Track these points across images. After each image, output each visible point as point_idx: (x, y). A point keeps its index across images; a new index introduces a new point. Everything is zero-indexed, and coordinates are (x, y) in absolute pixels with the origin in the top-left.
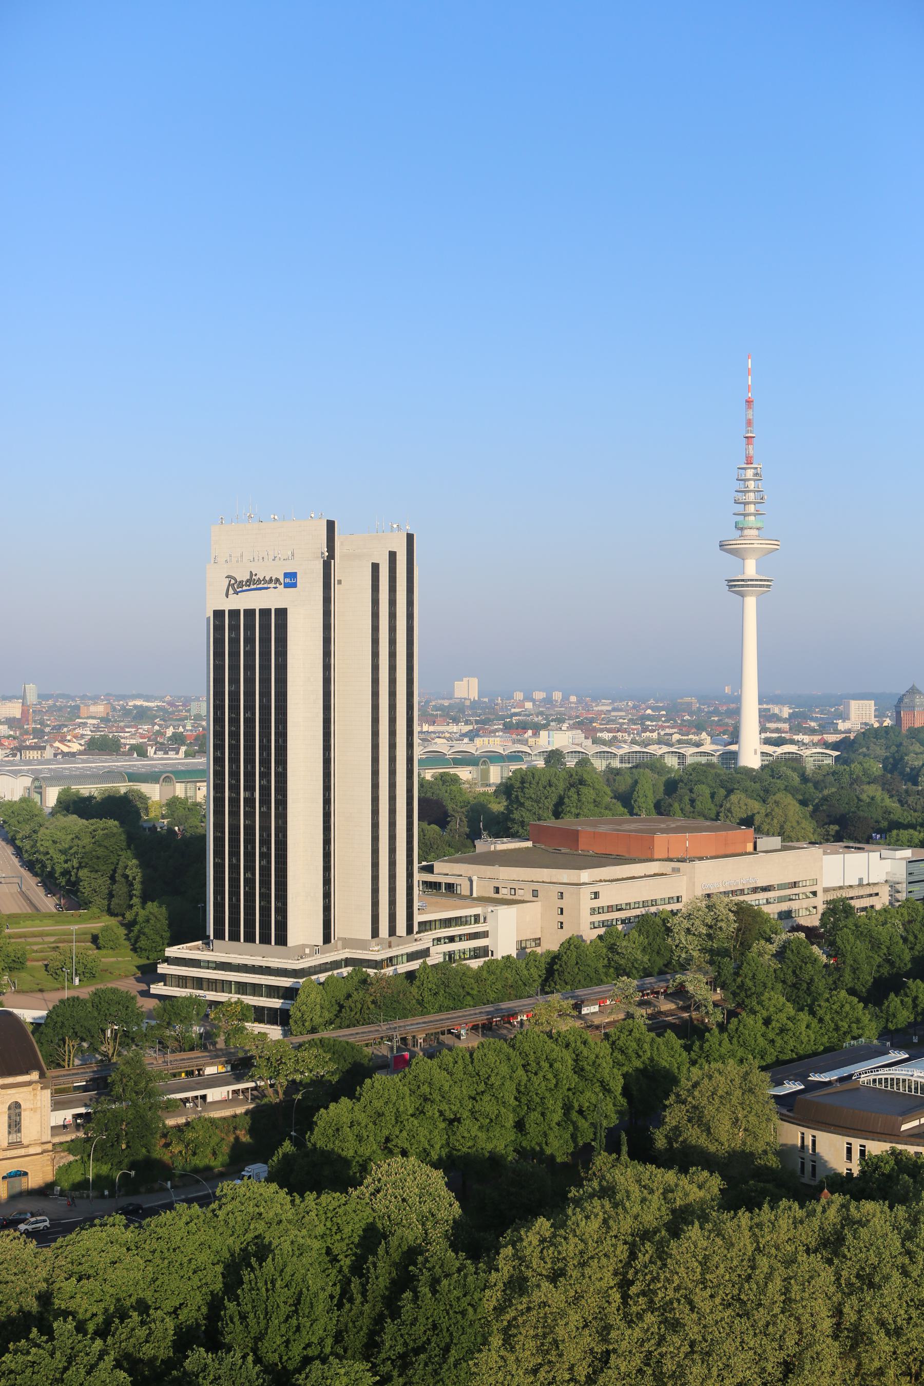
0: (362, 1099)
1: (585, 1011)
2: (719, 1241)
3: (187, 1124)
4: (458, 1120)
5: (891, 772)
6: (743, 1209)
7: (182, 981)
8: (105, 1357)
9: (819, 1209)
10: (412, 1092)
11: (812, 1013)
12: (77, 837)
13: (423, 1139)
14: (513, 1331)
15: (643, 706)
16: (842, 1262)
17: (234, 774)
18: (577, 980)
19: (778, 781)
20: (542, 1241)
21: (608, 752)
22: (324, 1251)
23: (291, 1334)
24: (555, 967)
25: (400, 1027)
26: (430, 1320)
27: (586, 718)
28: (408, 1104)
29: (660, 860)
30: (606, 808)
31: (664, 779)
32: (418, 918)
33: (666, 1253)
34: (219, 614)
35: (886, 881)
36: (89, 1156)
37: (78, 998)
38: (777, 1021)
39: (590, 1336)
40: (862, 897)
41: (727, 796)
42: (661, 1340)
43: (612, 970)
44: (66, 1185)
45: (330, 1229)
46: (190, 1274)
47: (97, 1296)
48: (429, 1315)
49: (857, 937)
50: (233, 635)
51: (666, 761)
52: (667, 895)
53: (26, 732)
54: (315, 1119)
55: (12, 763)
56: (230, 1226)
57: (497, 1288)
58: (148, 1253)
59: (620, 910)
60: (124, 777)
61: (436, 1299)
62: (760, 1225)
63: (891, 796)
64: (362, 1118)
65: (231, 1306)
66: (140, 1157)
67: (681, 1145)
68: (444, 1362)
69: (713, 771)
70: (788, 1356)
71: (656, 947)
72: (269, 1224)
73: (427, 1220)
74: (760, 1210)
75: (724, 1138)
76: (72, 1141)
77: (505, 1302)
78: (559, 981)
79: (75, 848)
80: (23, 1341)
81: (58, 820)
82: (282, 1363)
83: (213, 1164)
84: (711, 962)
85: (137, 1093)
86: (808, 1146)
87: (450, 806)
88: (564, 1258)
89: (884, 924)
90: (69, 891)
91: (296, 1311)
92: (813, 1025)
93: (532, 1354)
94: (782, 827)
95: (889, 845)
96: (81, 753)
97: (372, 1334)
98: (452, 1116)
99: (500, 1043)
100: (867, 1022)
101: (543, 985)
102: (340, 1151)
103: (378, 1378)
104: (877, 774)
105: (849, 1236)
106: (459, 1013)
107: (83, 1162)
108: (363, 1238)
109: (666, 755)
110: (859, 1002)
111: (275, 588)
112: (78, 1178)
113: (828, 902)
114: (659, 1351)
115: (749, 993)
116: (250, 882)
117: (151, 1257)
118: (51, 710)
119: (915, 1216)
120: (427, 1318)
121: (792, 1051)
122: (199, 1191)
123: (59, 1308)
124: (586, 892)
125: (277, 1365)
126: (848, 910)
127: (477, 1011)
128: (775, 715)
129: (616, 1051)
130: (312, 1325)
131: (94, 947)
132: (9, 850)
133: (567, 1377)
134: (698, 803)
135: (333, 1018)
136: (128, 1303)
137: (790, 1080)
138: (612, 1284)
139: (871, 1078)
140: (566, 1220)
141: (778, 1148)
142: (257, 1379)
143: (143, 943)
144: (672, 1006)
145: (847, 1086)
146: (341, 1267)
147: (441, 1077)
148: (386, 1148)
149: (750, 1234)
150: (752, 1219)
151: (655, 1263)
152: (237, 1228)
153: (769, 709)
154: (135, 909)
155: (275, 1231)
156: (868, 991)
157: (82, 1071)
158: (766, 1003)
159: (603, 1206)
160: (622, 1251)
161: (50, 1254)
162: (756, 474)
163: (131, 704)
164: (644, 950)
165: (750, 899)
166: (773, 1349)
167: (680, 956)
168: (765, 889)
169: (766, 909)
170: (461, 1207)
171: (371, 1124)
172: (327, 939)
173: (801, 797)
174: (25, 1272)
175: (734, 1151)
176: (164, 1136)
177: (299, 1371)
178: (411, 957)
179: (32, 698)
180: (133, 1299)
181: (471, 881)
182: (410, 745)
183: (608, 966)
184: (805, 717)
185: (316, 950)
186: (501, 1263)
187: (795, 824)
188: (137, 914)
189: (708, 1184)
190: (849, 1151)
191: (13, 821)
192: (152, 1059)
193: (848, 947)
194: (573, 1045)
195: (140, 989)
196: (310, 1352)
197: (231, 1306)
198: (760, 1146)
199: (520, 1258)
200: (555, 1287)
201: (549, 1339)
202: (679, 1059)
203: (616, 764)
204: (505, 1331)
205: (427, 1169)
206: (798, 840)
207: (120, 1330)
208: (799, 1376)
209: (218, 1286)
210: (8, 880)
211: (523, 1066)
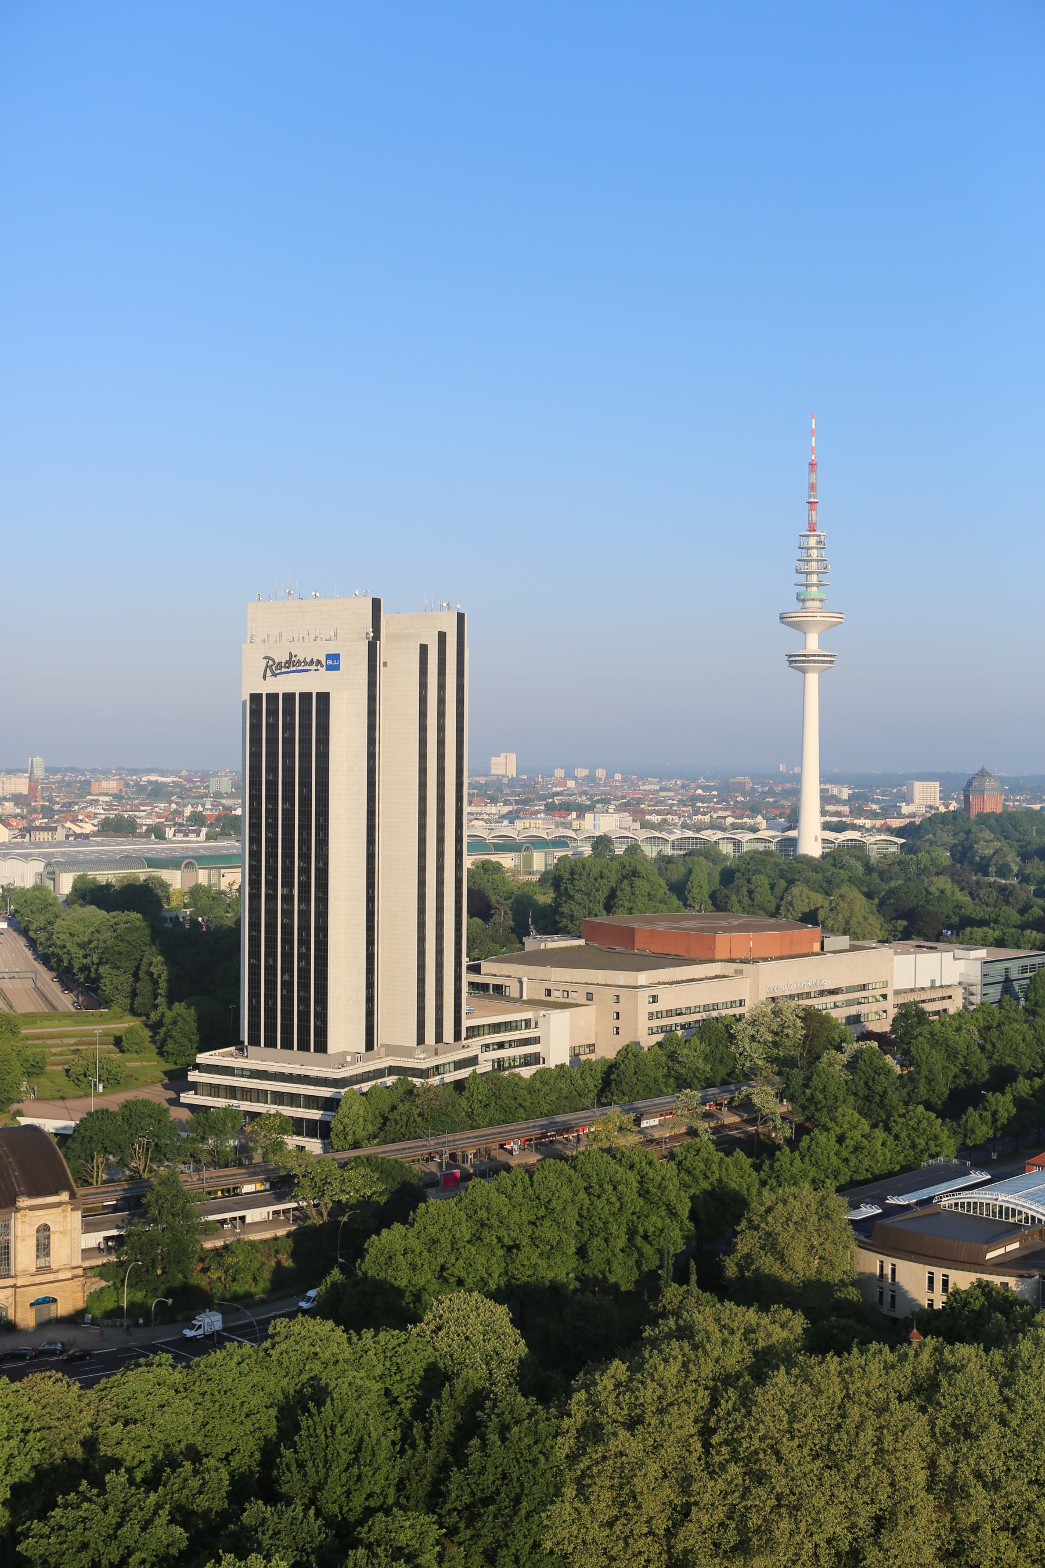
0: (416, 1225)
1: (644, 1124)
2: (807, 1388)
3: (226, 1247)
4: (517, 1247)
5: (960, 861)
6: (831, 1353)
7: (215, 1090)
8: (160, 1512)
9: (912, 1353)
10: (469, 1217)
11: (888, 1129)
12: (97, 931)
13: (480, 1268)
14: (588, 1481)
15: (693, 785)
16: (936, 1411)
17: (271, 870)
19: (841, 871)
20: (618, 1385)
22: (382, 1392)
23: (351, 1483)
24: (612, 1077)
25: (449, 1141)
26: (500, 1470)
27: (632, 799)
28: (464, 1229)
29: (721, 961)
30: (661, 902)
31: (719, 868)
32: (466, 1023)
33: (751, 1400)
34: (255, 698)
35: (960, 983)
36: (123, 1281)
37: (107, 1111)
38: (852, 1138)
39: (670, 1487)
40: (934, 1000)
41: (787, 889)
42: (746, 1492)
43: (672, 1080)
44: (98, 1313)
46: (243, 1418)
47: (144, 1443)
49: (933, 1046)
50: (271, 721)
52: (729, 999)
53: (34, 811)
54: (366, 1246)
55: (21, 846)
56: (284, 1366)
57: (570, 1435)
58: (198, 1396)
59: (679, 1014)
60: (142, 862)
62: (849, 1371)
63: (962, 889)
64: (416, 1244)
65: (288, 1454)
66: (177, 1284)
68: (515, 1514)
69: (772, 860)
70: (881, 1510)
71: (719, 1056)
72: (325, 1364)
73: (492, 1359)
75: (799, 1266)
76: (104, 1265)
77: (578, 1449)
78: (616, 1092)
80: (73, 1494)
81: (75, 912)
82: (342, 1515)
83: (253, 1290)
84: (779, 1073)
85: (173, 1215)
87: (493, 899)
88: (642, 1405)
89: (958, 1029)
90: (89, 988)
91: (356, 1459)
92: (889, 1143)
93: (608, 1506)
94: (847, 923)
95: (961, 943)
96: (95, 834)
97: (436, 1483)
98: (511, 1243)
99: (562, 1165)
100: (945, 1139)
101: (600, 1094)
103: (444, 1531)
104: (945, 864)
105: (945, 1383)
107: (116, 1289)
108: (424, 1379)
109: (721, 842)
110: (937, 1118)
112: (111, 1305)
113: (901, 1006)
114: (743, 1504)
115: (819, 1106)
116: (287, 985)
118: (63, 784)
119: (1012, 1360)
120: (496, 1467)
121: (867, 1170)
122: (239, 1320)
123: (105, 1455)
124: (644, 996)
125: (336, 1516)
126: (921, 1015)
127: (531, 1125)
128: (834, 797)
129: (683, 1172)
130: (374, 1474)
132: (22, 942)
133: (645, 1530)
134: (757, 897)
135: (377, 1131)
136: (177, 1449)
137: (867, 1203)
138: (693, 1431)
139: (953, 1202)
140: (643, 1364)
141: (856, 1277)
142: (319, 1534)
143: (170, 1046)
144: (737, 1119)
145: (928, 1210)
146: (401, 1409)
147: (499, 1201)
148: (440, 1276)
149: (839, 1379)
150: (841, 1364)
151: (739, 1410)
152: (292, 1369)
153: (827, 790)
154: (160, 1009)
155: (333, 1372)
156: (944, 1103)
157: (112, 1189)
158: (840, 1119)
159: (681, 1348)
160: (703, 1398)
161: (94, 1397)
162: (820, 542)
163: (144, 779)
164: (706, 1058)
165: (817, 1003)
166: (864, 1503)
167: (744, 1065)
168: (833, 992)
169: (835, 1014)
170: (527, 1345)
171: (425, 1252)
172: (370, 1045)
173: (866, 890)
174: (68, 1417)
175: (809, 1281)
176: (202, 1260)
177: (361, 1523)
178: (459, 1065)
179: (39, 773)
180: (183, 1445)
181: (521, 983)
183: (668, 1076)
184: (865, 798)
185: (357, 1058)
186: (573, 1408)
187: (861, 919)
188: (163, 1015)
189: (791, 1323)
190: (931, 1280)
191: (26, 911)
192: (189, 1178)
193: (924, 1057)
194: (638, 1166)
195: (168, 1097)
196: (372, 1503)
197: (288, 1454)
198: (836, 1276)
199: (593, 1403)
200: (633, 1435)
201: (626, 1490)
202: (749, 1180)
203: (668, 851)
204: (579, 1481)
205: (491, 1304)
206: (864, 938)
207: (172, 1481)
208: (892, 1531)
209: (273, 1431)
210: (21, 975)
211: (586, 1188)
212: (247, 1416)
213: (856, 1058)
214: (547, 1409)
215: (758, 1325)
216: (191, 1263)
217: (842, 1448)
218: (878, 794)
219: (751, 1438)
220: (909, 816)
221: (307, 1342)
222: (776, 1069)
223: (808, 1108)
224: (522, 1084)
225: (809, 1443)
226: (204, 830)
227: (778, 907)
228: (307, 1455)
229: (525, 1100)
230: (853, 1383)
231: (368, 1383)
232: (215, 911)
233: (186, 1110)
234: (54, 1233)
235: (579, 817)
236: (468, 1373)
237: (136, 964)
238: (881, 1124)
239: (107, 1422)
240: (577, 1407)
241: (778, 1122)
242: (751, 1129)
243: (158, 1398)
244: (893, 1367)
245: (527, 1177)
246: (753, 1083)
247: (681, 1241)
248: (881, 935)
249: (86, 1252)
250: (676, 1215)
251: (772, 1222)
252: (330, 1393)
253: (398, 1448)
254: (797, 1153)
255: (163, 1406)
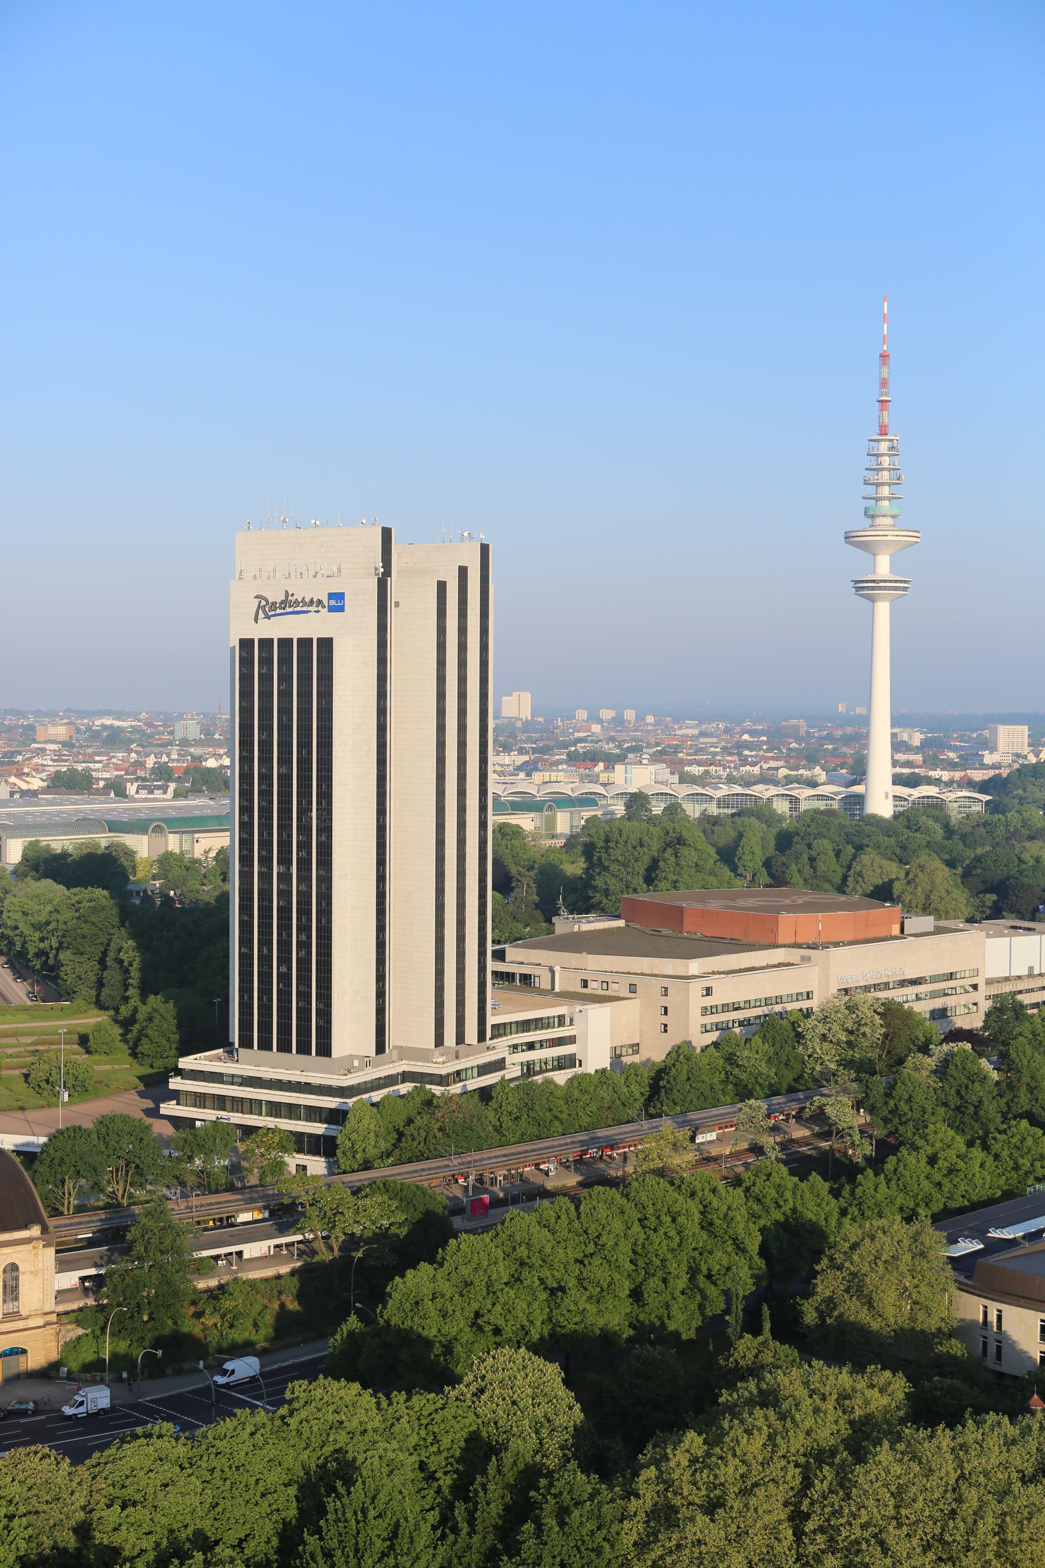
0: (446, 1264)
1: (700, 1139)
3: (221, 1287)
4: (562, 1289)
7: (200, 1100)
11: (986, 1148)
13: (521, 1314)
15: (738, 729)
17: (266, 844)
18: (688, 1099)
19: (918, 835)
20: (693, 1461)
21: (702, 795)
22: (417, 1466)
24: (662, 1083)
25: (476, 1161)
27: (668, 746)
28: (501, 1269)
30: (710, 874)
32: (491, 1020)
33: (850, 1480)
34: (246, 644)
36: (103, 1329)
37: (80, 1128)
38: (945, 1159)
40: (1032, 990)
41: (855, 857)
43: (730, 1087)
44: (75, 1366)
45: (424, 1439)
46: (258, 1498)
47: (147, 1529)
48: (556, 1553)
49: (1035, 1048)
50: (264, 671)
51: (775, 806)
54: (388, 1289)
56: (304, 1437)
57: (638, 1518)
58: (205, 1472)
60: (103, 826)
61: (564, 1533)
64: (446, 1287)
65: (312, 1541)
66: (167, 1331)
67: (836, 1320)
71: (784, 1058)
72: (352, 1434)
73: (542, 1426)
74: (964, 1426)
75: (890, 1312)
76: (80, 1309)
77: (648, 1536)
79: (54, 923)
83: (254, 1338)
84: (857, 1080)
86: (992, 1322)
87: (513, 870)
88: (723, 1485)
91: (391, 1547)
92: (988, 1164)
94: (927, 897)
96: (45, 791)
98: (555, 1285)
99: (612, 1193)
101: (646, 1106)
102: (420, 1329)
104: (1039, 825)
106: (547, 1143)
107: (96, 1338)
108: (465, 1450)
109: (775, 799)
111: (317, 612)
112: (90, 1357)
115: (904, 1119)
116: (285, 978)
117: (209, 1478)
120: (554, 1557)
121: (963, 1196)
123: (101, 1544)
124: (696, 988)
126: (1019, 1009)
127: (569, 1141)
129: (751, 1200)
131: (82, 1050)
134: (822, 867)
135: (391, 1148)
141: (955, 1324)
143: (145, 1047)
144: (807, 1133)
146: (439, 1487)
149: (952, 1457)
150: (954, 1438)
152: (313, 1440)
155: (361, 1443)
157: (87, 1219)
158: (931, 1137)
159: (766, 1418)
162: (892, 448)
163: (97, 723)
164: (769, 1061)
165: (897, 995)
167: (813, 1069)
168: (914, 982)
170: (582, 1410)
171: (457, 1295)
172: (380, 1048)
173: (947, 857)
174: (58, 1500)
175: (901, 1329)
176: (194, 1303)
178: (484, 1069)
180: (190, 1531)
181: (553, 972)
182: (483, 808)
183: (726, 1082)
185: (367, 1062)
187: (944, 894)
188: (135, 1010)
193: (1025, 1062)
194: (700, 1194)
195: (145, 1106)
197: (312, 1541)
198: (932, 1324)
199: (665, 1482)
200: (713, 1521)
203: (713, 810)
205: (539, 1361)
209: (292, 1513)
211: (640, 1220)
212: (263, 1495)
213: (946, 1062)
214: (611, 1488)
215: (853, 1389)
216: (182, 1306)
217: (959, 1538)
218: (955, 740)
219: (851, 1525)
220: (994, 767)
221: (331, 1409)
222: (853, 1075)
223: (891, 1121)
224: (558, 1093)
225: (920, 1532)
226: (172, 786)
227: (845, 878)
228: (334, 1543)
229: (561, 1112)
230: (968, 1462)
231: (402, 1456)
232: (190, 883)
233: (166, 1122)
234: (24, 1273)
235: (606, 768)
236: (515, 1444)
237: (102, 949)
238: (978, 1141)
239: (102, 1505)
240: (645, 1486)
241: (857, 1137)
242: (824, 1145)
243: (160, 1476)
244: (1014, 1442)
245: (573, 1208)
246: (825, 1091)
247: (750, 1281)
248: (968, 911)
249: (61, 1295)
250: (744, 1251)
251: (860, 1262)
252: (358, 1468)
253: (439, 1532)
254: (882, 1176)
255: (167, 1485)
